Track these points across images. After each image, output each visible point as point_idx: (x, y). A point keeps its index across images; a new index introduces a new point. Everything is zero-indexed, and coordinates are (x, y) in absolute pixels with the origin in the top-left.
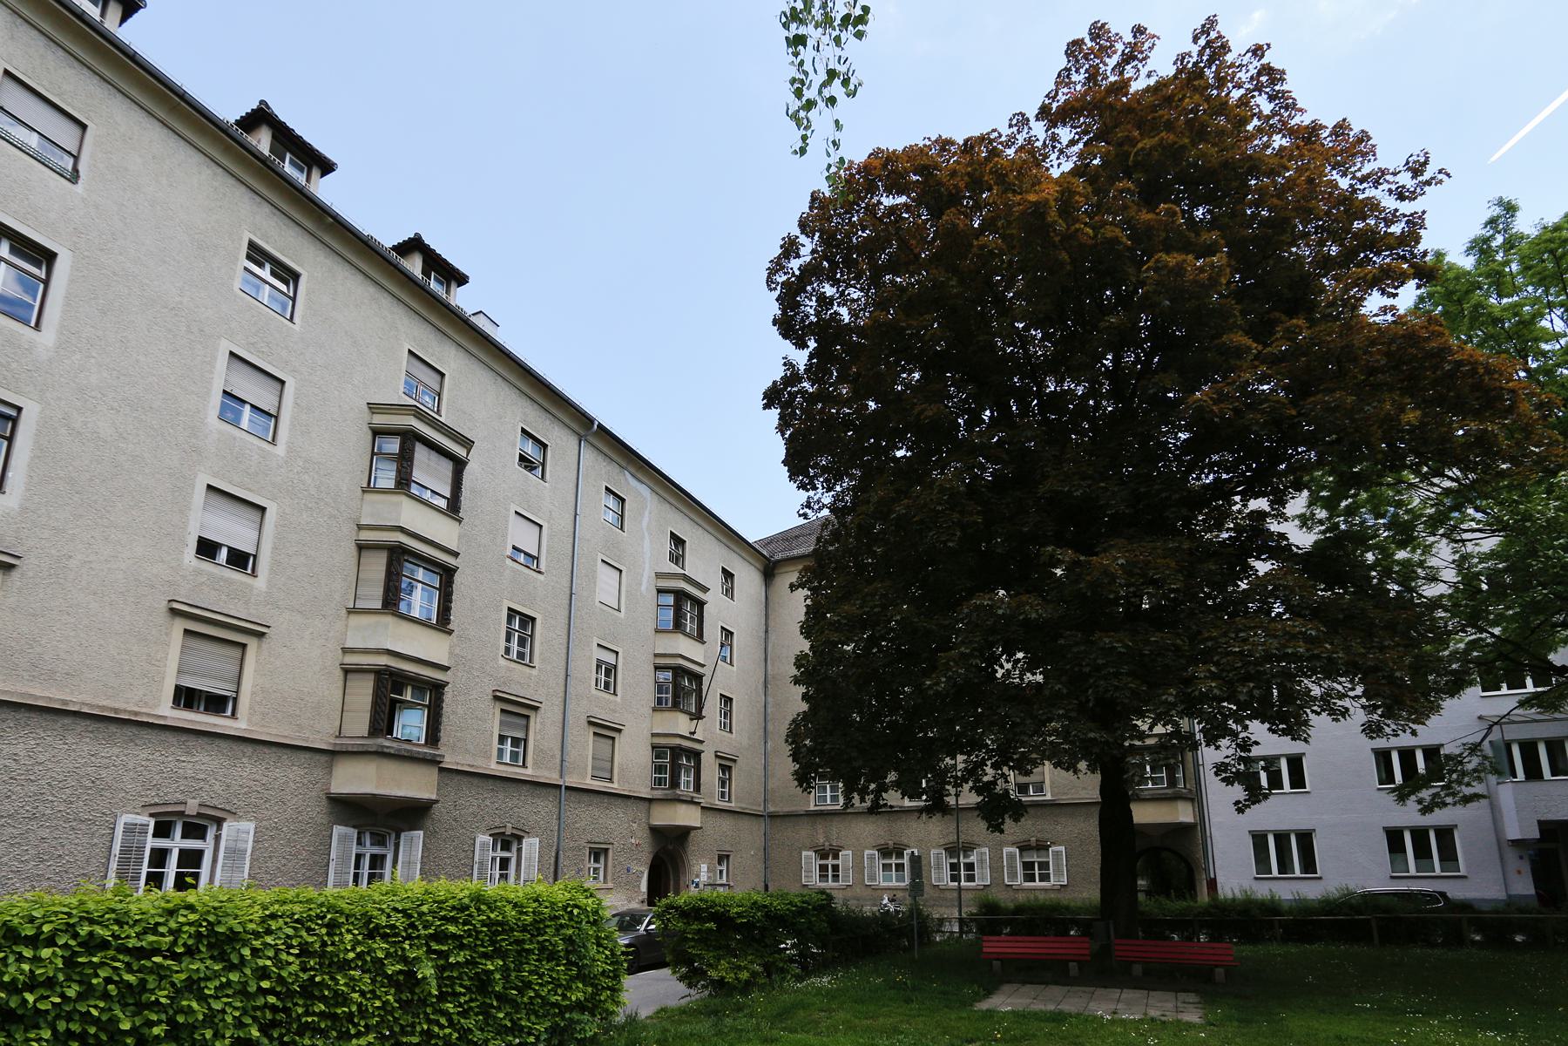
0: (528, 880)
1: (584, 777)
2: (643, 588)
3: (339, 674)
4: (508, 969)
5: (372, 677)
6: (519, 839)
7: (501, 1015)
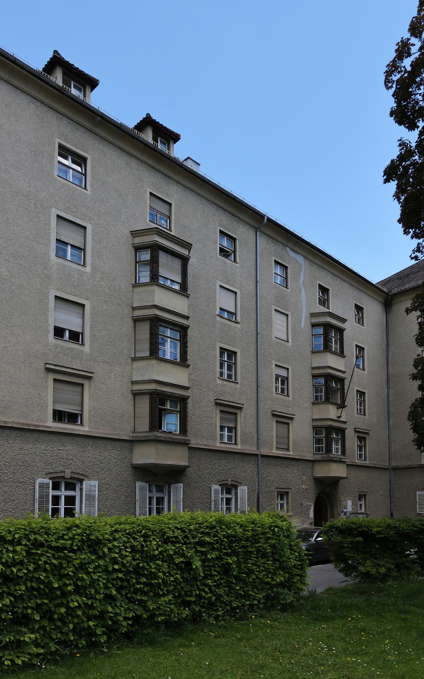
0: (242, 511)
1: (272, 449)
2: (302, 325)
3: (130, 396)
4: (240, 562)
5: (148, 397)
6: (236, 487)
7: (238, 588)
